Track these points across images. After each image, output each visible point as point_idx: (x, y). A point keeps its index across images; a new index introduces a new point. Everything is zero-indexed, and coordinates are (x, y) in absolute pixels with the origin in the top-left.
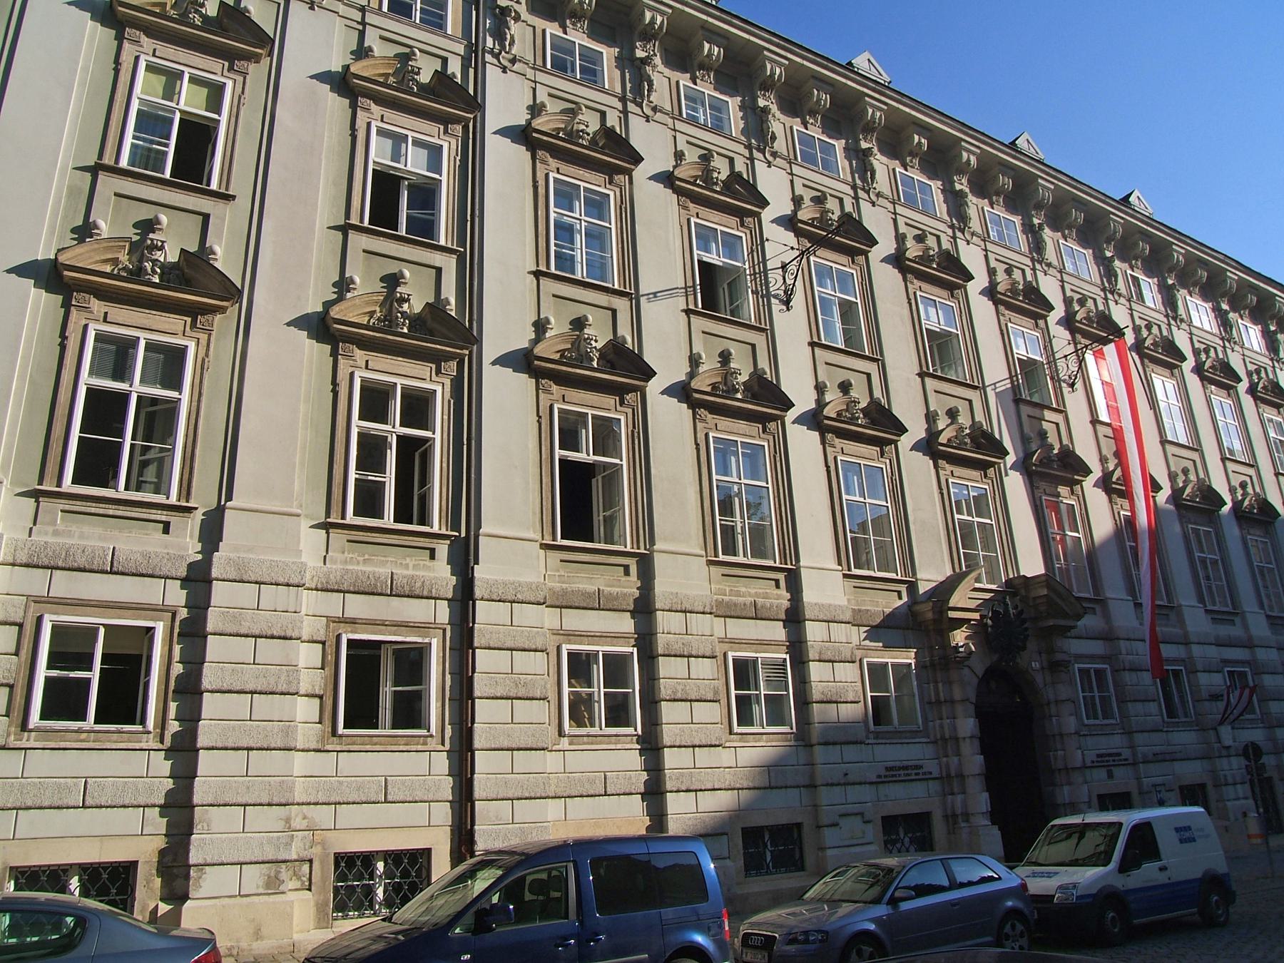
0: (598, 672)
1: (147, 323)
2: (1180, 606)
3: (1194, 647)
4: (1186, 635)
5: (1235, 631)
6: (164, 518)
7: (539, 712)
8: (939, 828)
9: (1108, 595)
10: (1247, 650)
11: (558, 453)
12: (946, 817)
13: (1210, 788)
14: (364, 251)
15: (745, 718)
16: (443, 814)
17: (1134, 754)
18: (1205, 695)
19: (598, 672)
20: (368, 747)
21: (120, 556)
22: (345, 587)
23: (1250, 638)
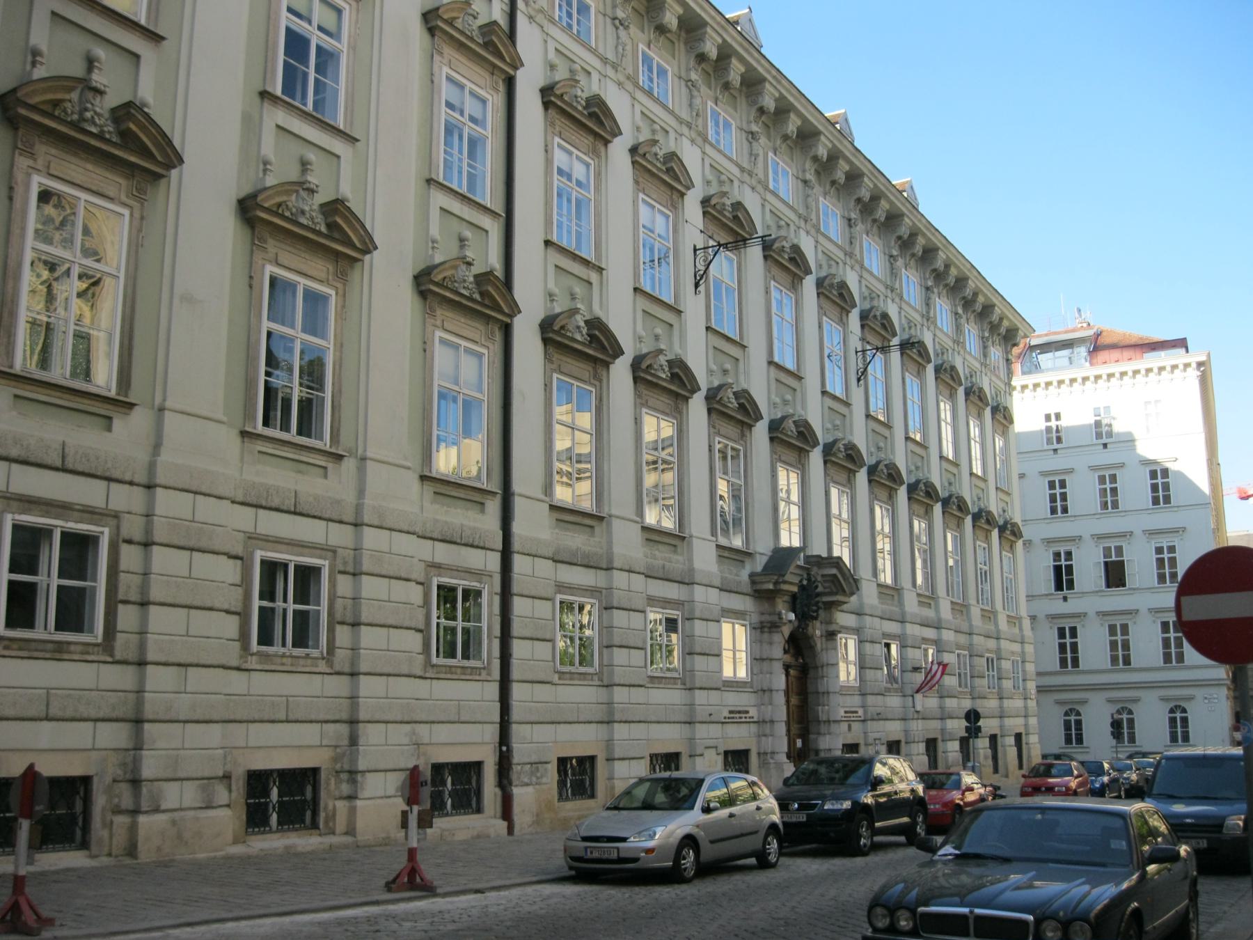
0: (52, 555)
1: (304, 268)
2: (691, 536)
3: (868, 619)
4: (903, 614)
5: (676, 562)
6: (323, 464)
7: (413, 641)
8: (754, 759)
9: (613, 512)
10: (934, 631)
11: (266, 325)
12: (759, 754)
13: (903, 744)
14: (278, 126)
15: (266, 638)
16: (491, 733)
17: (865, 712)
18: (910, 668)
19: (52, 555)
20: (449, 676)
21: (70, 451)
22: (435, 535)
23: (940, 620)
